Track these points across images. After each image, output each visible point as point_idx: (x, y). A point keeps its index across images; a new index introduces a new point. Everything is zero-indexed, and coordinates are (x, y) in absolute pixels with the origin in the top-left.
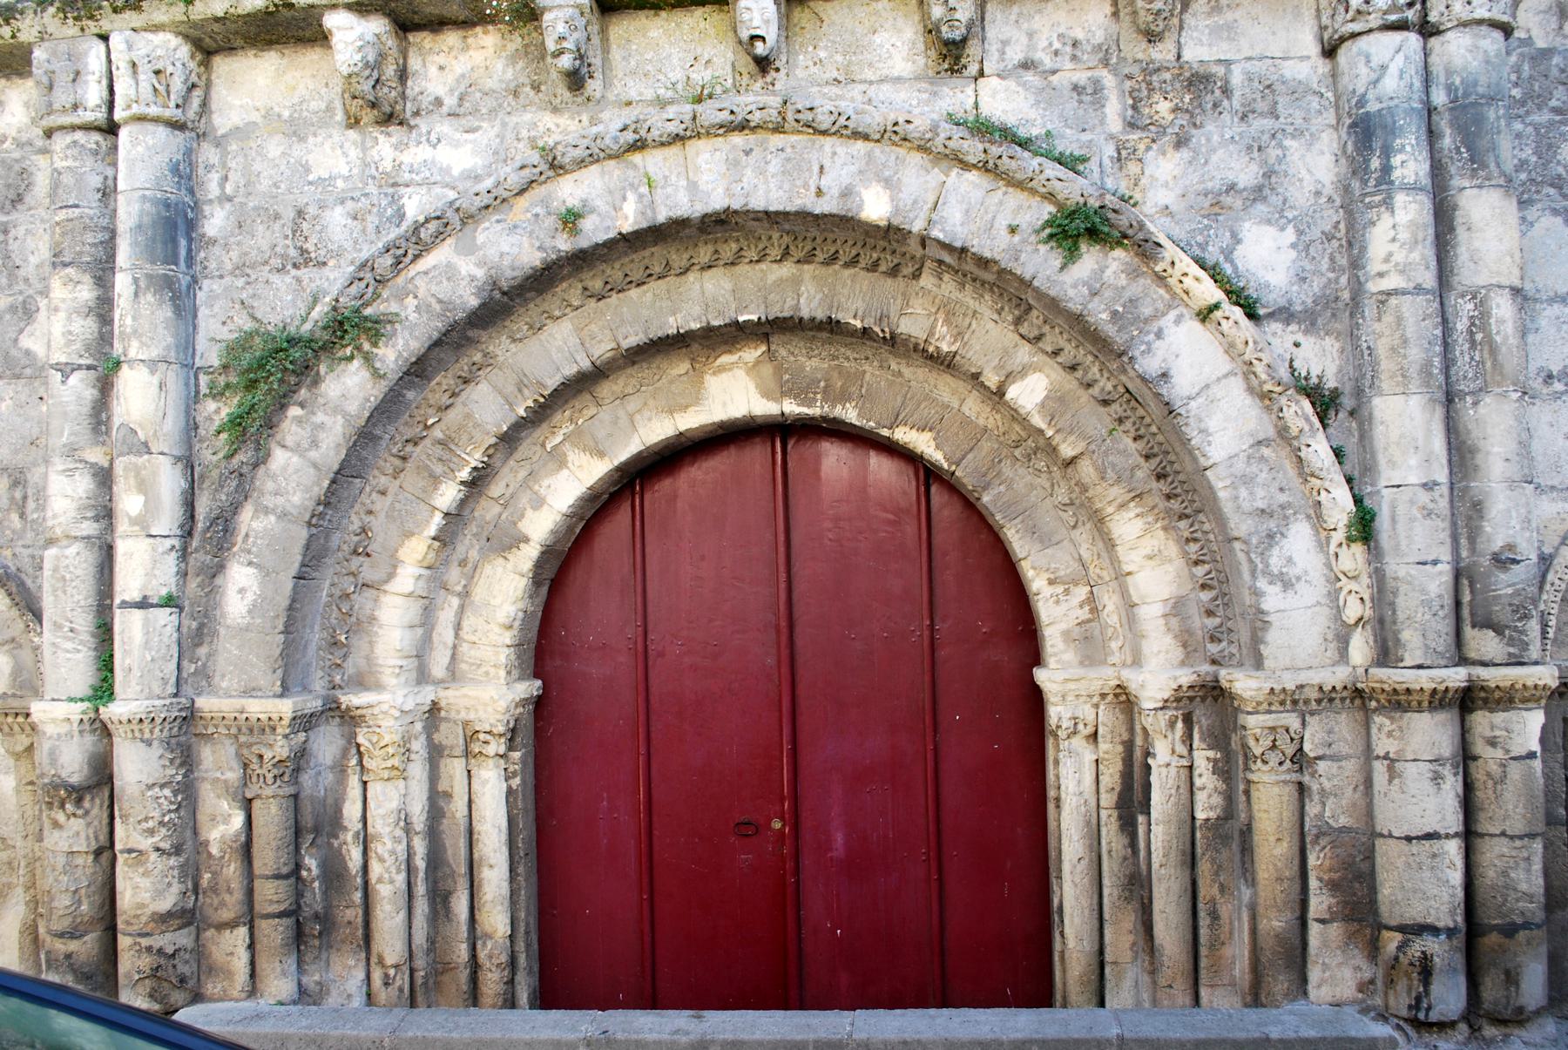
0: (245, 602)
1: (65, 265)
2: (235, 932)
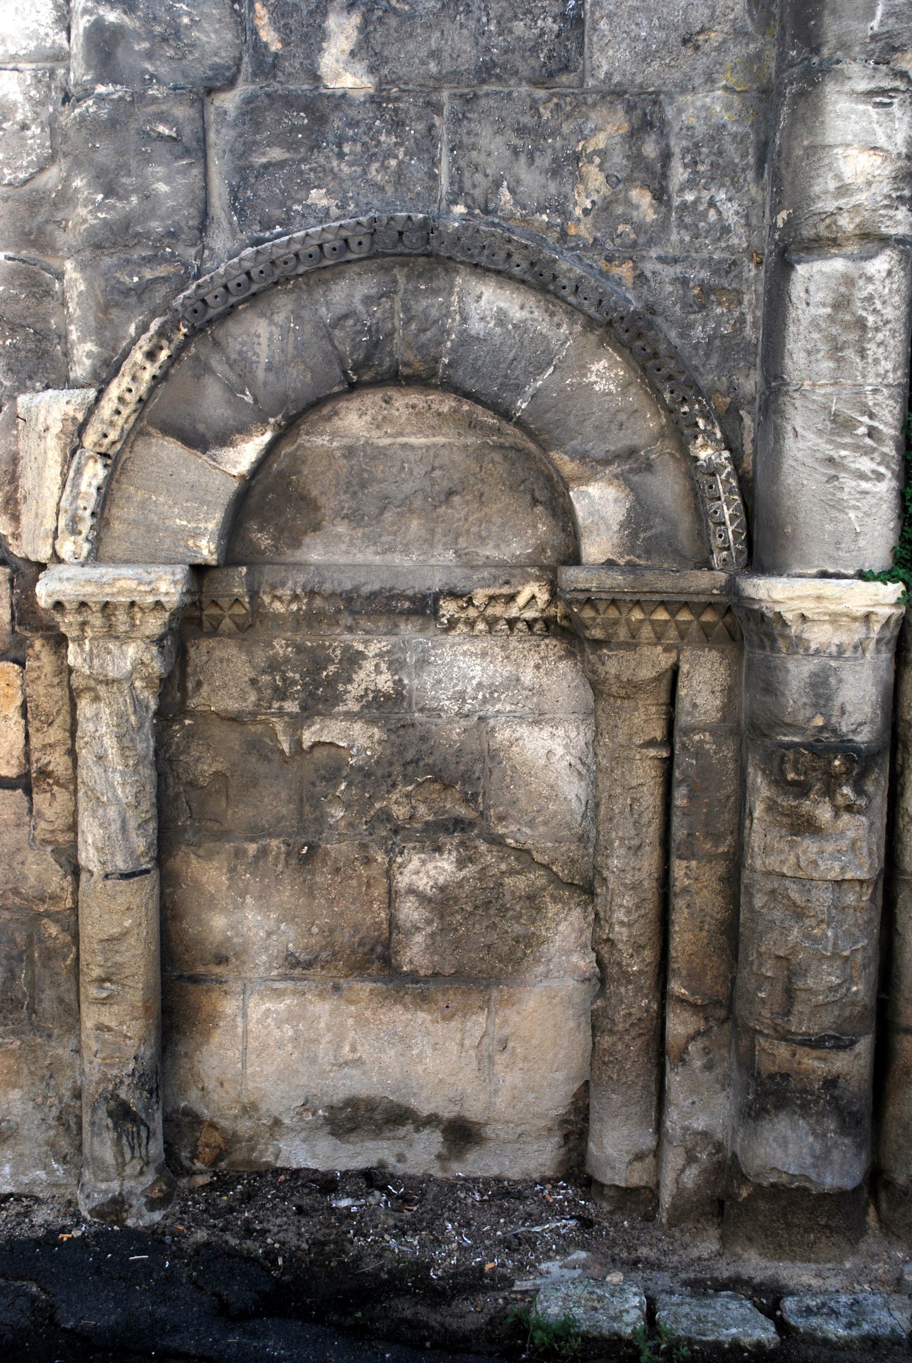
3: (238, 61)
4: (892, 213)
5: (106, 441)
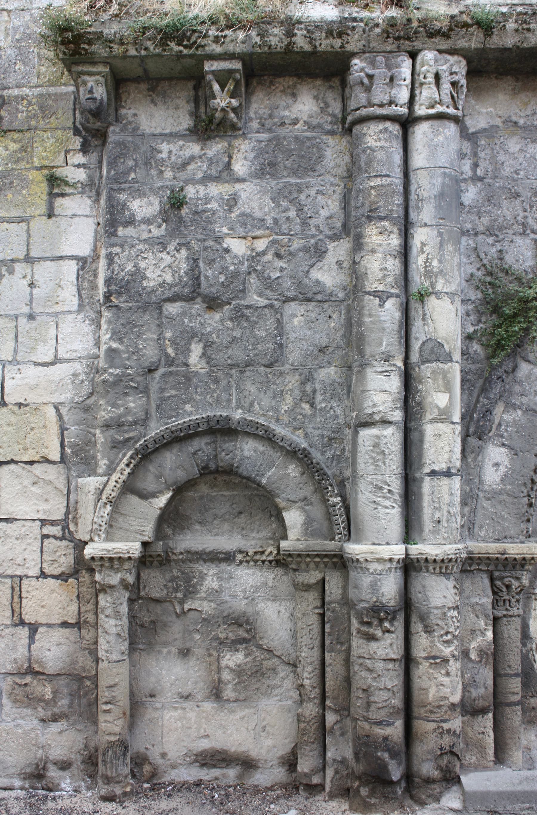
0: (499, 473)
1: (381, 219)
2: (485, 716)
3: (160, 360)
4: (392, 413)
5: (111, 497)
